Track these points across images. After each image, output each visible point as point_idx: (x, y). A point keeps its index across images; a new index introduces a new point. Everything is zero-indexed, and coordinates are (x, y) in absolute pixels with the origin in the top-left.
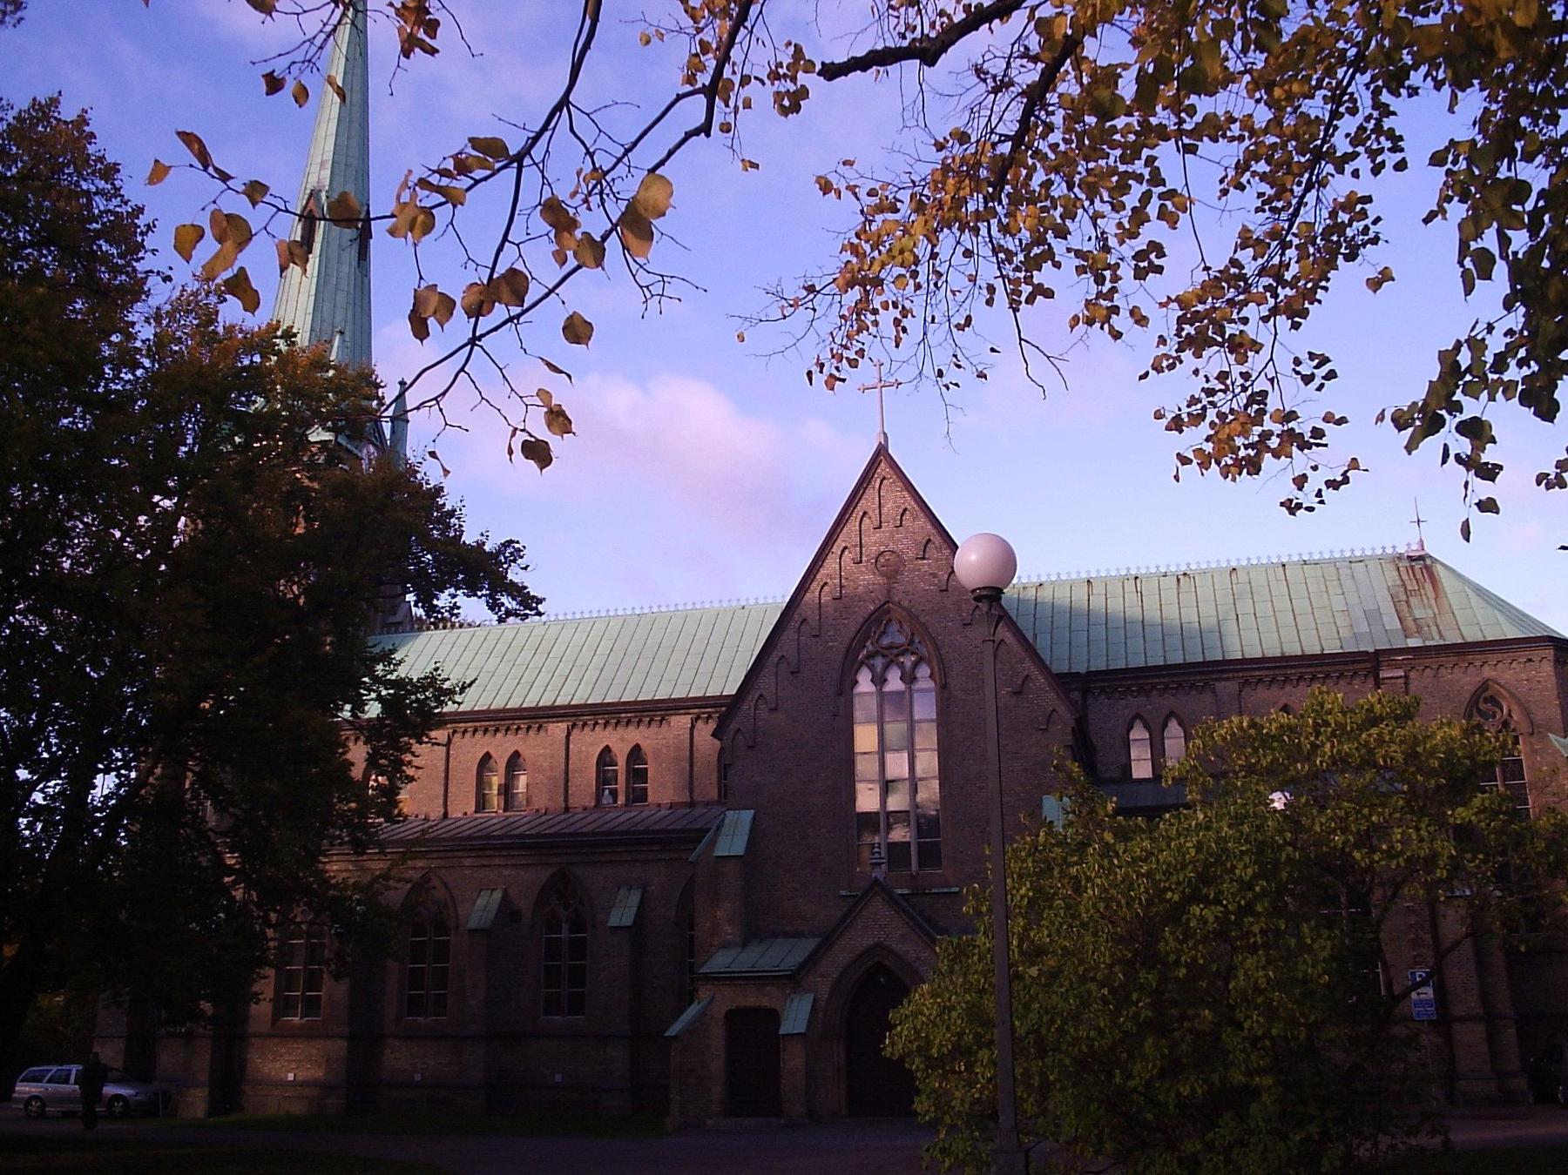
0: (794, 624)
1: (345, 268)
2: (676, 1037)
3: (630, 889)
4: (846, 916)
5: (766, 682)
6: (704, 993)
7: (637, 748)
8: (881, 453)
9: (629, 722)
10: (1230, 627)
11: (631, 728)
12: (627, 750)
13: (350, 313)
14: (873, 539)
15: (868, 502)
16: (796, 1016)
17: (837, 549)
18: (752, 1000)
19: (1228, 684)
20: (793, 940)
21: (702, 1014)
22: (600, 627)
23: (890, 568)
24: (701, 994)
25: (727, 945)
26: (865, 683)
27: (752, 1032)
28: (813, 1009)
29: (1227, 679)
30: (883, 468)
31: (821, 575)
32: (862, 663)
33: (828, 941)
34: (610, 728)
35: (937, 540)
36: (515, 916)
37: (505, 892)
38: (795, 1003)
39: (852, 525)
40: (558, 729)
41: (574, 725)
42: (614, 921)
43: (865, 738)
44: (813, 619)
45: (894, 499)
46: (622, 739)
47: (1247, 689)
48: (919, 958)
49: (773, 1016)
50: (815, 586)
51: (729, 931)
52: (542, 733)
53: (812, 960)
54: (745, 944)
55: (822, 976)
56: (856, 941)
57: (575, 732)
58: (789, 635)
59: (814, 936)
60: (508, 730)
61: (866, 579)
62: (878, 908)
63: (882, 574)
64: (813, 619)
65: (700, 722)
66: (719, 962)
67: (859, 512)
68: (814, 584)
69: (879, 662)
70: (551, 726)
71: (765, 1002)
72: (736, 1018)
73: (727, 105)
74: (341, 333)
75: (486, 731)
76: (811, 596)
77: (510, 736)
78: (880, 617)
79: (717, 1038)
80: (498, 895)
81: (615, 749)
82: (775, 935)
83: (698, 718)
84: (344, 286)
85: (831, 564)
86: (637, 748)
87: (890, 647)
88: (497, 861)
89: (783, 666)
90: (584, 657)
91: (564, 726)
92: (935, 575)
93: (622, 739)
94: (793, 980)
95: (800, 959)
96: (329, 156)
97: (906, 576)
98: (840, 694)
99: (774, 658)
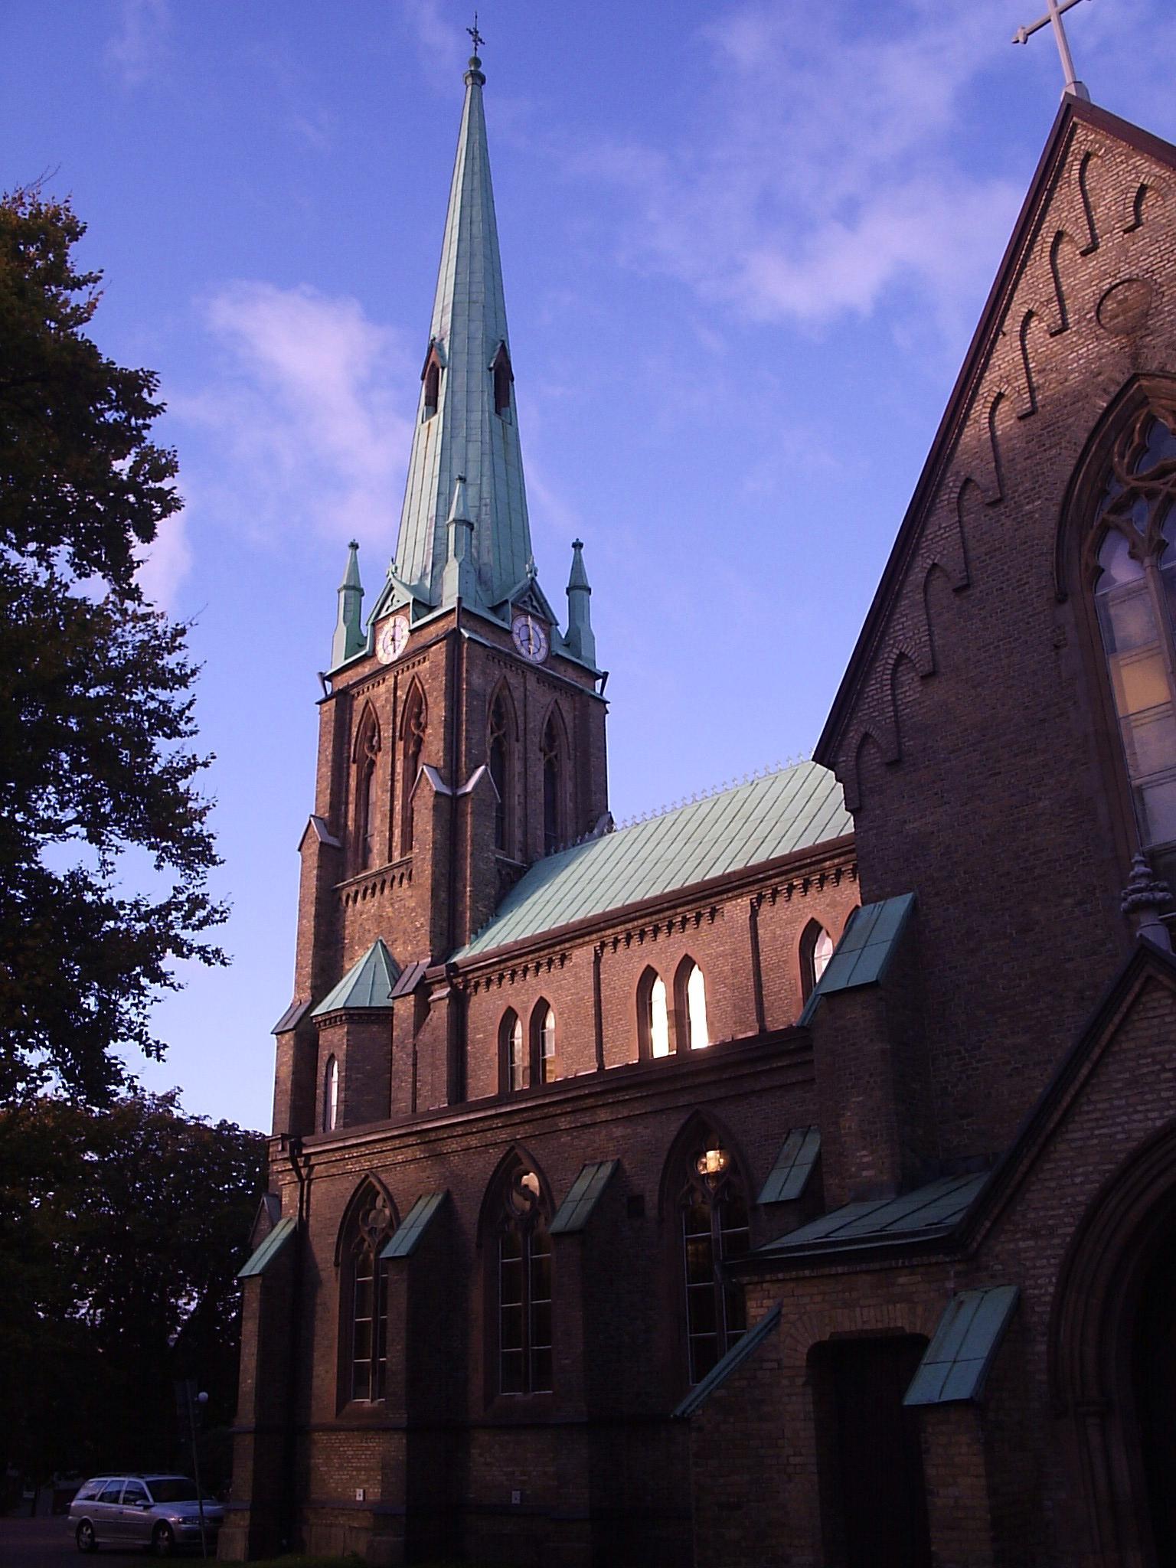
0: (948, 496)
1: (477, 416)
5: (908, 630)
13: (487, 464)
14: (1083, 275)
15: (1066, 209)
30: (1084, 138)
31: (988, 388)
34: (812, 891)
36: (636, 1204)
37: (618, 1168)
38: (967, 1311)
39: (1038, 266)
40: (737, 909)
41: (760, 898)
44: (984, 477)
50: (980, 411)
52: (718, 921)
55: (1035, 1234)
57: (765, 910)
60: (670, 926)
61: (1079, 358)
63: (1115, 332)
64: (984, 477)
67: (1047, 237)
68: (978, 406)
70: (728, 906)
71: (900, 1318)
74: (462, 479)
75: (642, 935)
76: (975, 431)
77: (676, 935)
80: (606, 1170)
84: (476, 435)
85: (1005, 356)
88: (603, 1115)
89: (938, 583)
91: (745, 902)
94: (957, 1253)
96: (450, 299)
98: (1061, 599)
99: (917, 575)
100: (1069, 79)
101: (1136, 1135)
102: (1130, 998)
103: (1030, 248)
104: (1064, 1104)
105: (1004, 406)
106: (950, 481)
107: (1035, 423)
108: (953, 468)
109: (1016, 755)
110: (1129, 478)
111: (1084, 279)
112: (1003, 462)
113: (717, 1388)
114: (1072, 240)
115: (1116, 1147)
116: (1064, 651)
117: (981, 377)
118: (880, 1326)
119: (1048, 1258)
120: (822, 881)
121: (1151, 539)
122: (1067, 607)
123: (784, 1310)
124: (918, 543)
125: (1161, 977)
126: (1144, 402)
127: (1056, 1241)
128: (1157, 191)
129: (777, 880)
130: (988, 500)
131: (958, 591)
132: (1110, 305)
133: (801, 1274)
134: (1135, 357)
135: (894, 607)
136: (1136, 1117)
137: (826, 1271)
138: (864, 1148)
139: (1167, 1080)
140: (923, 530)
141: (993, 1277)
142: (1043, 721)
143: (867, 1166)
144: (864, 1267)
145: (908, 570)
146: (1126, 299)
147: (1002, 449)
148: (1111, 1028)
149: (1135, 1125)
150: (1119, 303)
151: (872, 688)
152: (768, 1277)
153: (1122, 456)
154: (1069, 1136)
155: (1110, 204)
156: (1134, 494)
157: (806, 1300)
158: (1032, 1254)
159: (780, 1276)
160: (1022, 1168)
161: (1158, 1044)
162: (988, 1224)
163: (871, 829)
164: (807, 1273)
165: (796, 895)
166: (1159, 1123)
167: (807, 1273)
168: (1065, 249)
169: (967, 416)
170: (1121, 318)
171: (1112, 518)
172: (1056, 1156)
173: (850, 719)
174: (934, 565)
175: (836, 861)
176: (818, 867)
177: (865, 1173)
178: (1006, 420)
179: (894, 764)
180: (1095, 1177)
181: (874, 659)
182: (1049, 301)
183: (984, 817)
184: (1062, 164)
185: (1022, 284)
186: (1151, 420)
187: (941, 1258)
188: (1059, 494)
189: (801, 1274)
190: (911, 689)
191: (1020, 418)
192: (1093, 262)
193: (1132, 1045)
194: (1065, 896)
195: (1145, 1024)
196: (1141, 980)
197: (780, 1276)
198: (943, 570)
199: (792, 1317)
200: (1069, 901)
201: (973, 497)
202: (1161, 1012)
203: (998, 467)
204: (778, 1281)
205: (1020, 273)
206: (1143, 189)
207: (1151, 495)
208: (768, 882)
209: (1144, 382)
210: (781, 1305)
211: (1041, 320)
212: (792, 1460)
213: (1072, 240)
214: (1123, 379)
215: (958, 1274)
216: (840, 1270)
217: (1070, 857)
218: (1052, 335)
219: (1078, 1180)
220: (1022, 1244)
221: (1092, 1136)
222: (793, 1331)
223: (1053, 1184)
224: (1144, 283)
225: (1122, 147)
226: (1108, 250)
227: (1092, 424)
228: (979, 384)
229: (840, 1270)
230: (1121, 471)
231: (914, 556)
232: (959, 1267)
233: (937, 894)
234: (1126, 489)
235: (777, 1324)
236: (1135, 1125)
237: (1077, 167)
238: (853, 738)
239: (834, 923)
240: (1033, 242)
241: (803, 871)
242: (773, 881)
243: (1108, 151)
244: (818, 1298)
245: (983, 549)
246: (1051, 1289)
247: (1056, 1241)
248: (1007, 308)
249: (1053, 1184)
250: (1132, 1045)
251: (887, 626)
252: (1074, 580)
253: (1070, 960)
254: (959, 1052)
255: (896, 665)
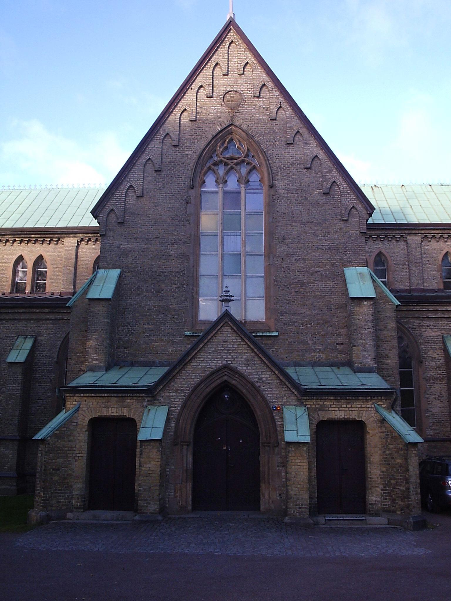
0: (160, 136)
2: (42, 441)
3: (25, 338)
4: (188, 354)
5: (135, 178)
6: (71, 403)
7: (41, 258)
8: (231, 24)
9: (36, 241)
10: (408, 211)
11: (38, 245)
12: (34, 258)
15: (220, 56)
16: (153, 424)
17: (195, 86)
18: (113, 409)
19: (414, 237)
20: (147, 368)
21: (68, 422)
22: (24, 194)
23: (234, 102)
24: (68, 404)
25: (92, 369)
26: (210, 182)
27: (113, 438)
28: (168, 421)
29: (415, 234)
30: (232, 35)
31: (182, 104)
32: (209, 168)
33: (176, 368)
34: (23, 244)
35: (270, 84)
39: (207, 71)
42: (11, 358)
43: (208, 221)
44: (174, 135)
45: (239, 56)
46: (31, 251)
47: (425, 242)
48: (260, 379)
49: (130, 425)
50: (177, 112)
51: (95, 358)
53: (165, 381)
54: (108, 368)
55: (176, 391)
56: (208, 362)
58: (155, 143)
59: (162, 365)
61: (215, 110)
62: (227, 336)
63: (227, 106)
64: (174, 135)
65: (83, 243)
66: (86, 379)
69: (222, 170)
71: (125, 412)
72: (97, 424)
73: (93, 273)
76: (174, 117)
78: (225, 135)
79: (81, 441)
81: (26, 257)
82: (133, 364)
83: (82, 240)
85: (190, 97)
86: (41, 258)
87: (231, 159)
90: (12, 208)
92: (267, 109)
93: (31, 251)
94: (150, 394)
95: (156, 378)
97: (245, 109)
98: (192, 188)
100: (230, 11)
101: (213, 367)
102: (219, 327)
103: (207, 64)
104: (193, 354)
105: (185, 114)
106: (161, 131)
107: (195, 125)
108: (163, 128)
109: (166, 234)
110: (221, 156)
111: (222, 84)
112: (181, 133)
113: (56, 430)
114: (221, 68)
115: (206, 369)
116: (189, 205)
117: (180, 100)
118: (118, 414)
119: (179, 399)
120: (28, 242)
121: (224, 178)
122: (193, 191)
123: (81, 406)
124: (145, 149)
125: (230, 323)
126: (231, 133)
127: (183, 394)
128: (252, 67)
129: (10, 236)
130: (174, 144)
131: (156, 171)
132: (228, 96)
133: (90, 395)
134: (232, 118)
135: (132, 168)
136: (214, 362)
137: (101, 395)
138: (95, 354)
139: (225, 353)
140: (148, 145)
141: (160, 403)
142: (177, 225)
143: (96, 360)
144: (115, 395)
145: (140, 156)
146: (233, 97)
147: (182, 128)
148: (212, 335)
149: (213, 364)
150: (231, 97)
151: (118, 194)
152: (77, 395)
153: (220, 148)
154: (192, 364)
155: (236, 62)
156: (221, 162)
157: (91, 404)
158: (175, 397)
159: (82, 395)
160: (176, 371)
161: (224, 342)
162: (161, 387)
163: (108, 243)
164: (93, 395)
165: (16, 244)
166: (220, 365)
167: (93, 395)
168: (217, 69)
169: (172, 112)
170: (230, 102)
171: (213, 167)
172: (187, 369)
173: (107, 202)
174: (150, 159)
175: (37, 236)
176: (29, 236)
177: (94, 362)
178: (185, 119)
179: (121, 223)
180: (198, 377)
181: (121, 184)
182: (209, 85)
183: (150, 251)
184: (224, 40)
185: (201, 74)
186: (231, 140)
187: (144, 395)
188: (198, 152)
189: (90, 395)
190: (132, 198)
191: (190, 121)
192: (225, 80)
193: (217, 341)
194: (174, 284)
195: (222, 335)
196: (224, 322)
197: (82, 395)
198: (152, 161)
199: (84, 409)
200: (175, 286)
201: (168, 140)
202: (227, 333)
203: (179, 134)
204: (81, 396)
205: (201, 70)
206: (247, 63)
207: (226, 164)
208: (5, 236)
209: (233, 127)
210: (80, 404)
211: (205, 90)
212: (78, 455)
213: (221, 68)
214: (228, 123)
215: (148, 401)
216: (106, 395)
217: (178, 272)
218: (207, 97)
219: (193, 377)
220: (171, 394)
221: (199, 365)
222: (84, 413)
223: (185, 378)
224: (240, 94)
225: (244, 46)
226: (232, 78)
227: (214, 134)
228: (179, 102)
229: (106, 395)
230: (219, 152)
231: (143, 152)
232: (149, 399)
233: (129, 272)
234: (219, 159)
235: (78, 410)
236: (213, 364)
237: (228, 44)
238: (107, 209)
239: (30, 259)
240: (208, 62)
241: (21, 236)
242: (8, 236)
243: (239, 44)
244: (95, 404)
245: (168, 160)
246: (179, 408)
247: (183, 394)
248: (194, 81)
249: (185, 378)
250: (217, 341)
251: (128, 174)
252: (195, 183)
253: (172, 305)
254: (128, 326)
255: (129, 189)
